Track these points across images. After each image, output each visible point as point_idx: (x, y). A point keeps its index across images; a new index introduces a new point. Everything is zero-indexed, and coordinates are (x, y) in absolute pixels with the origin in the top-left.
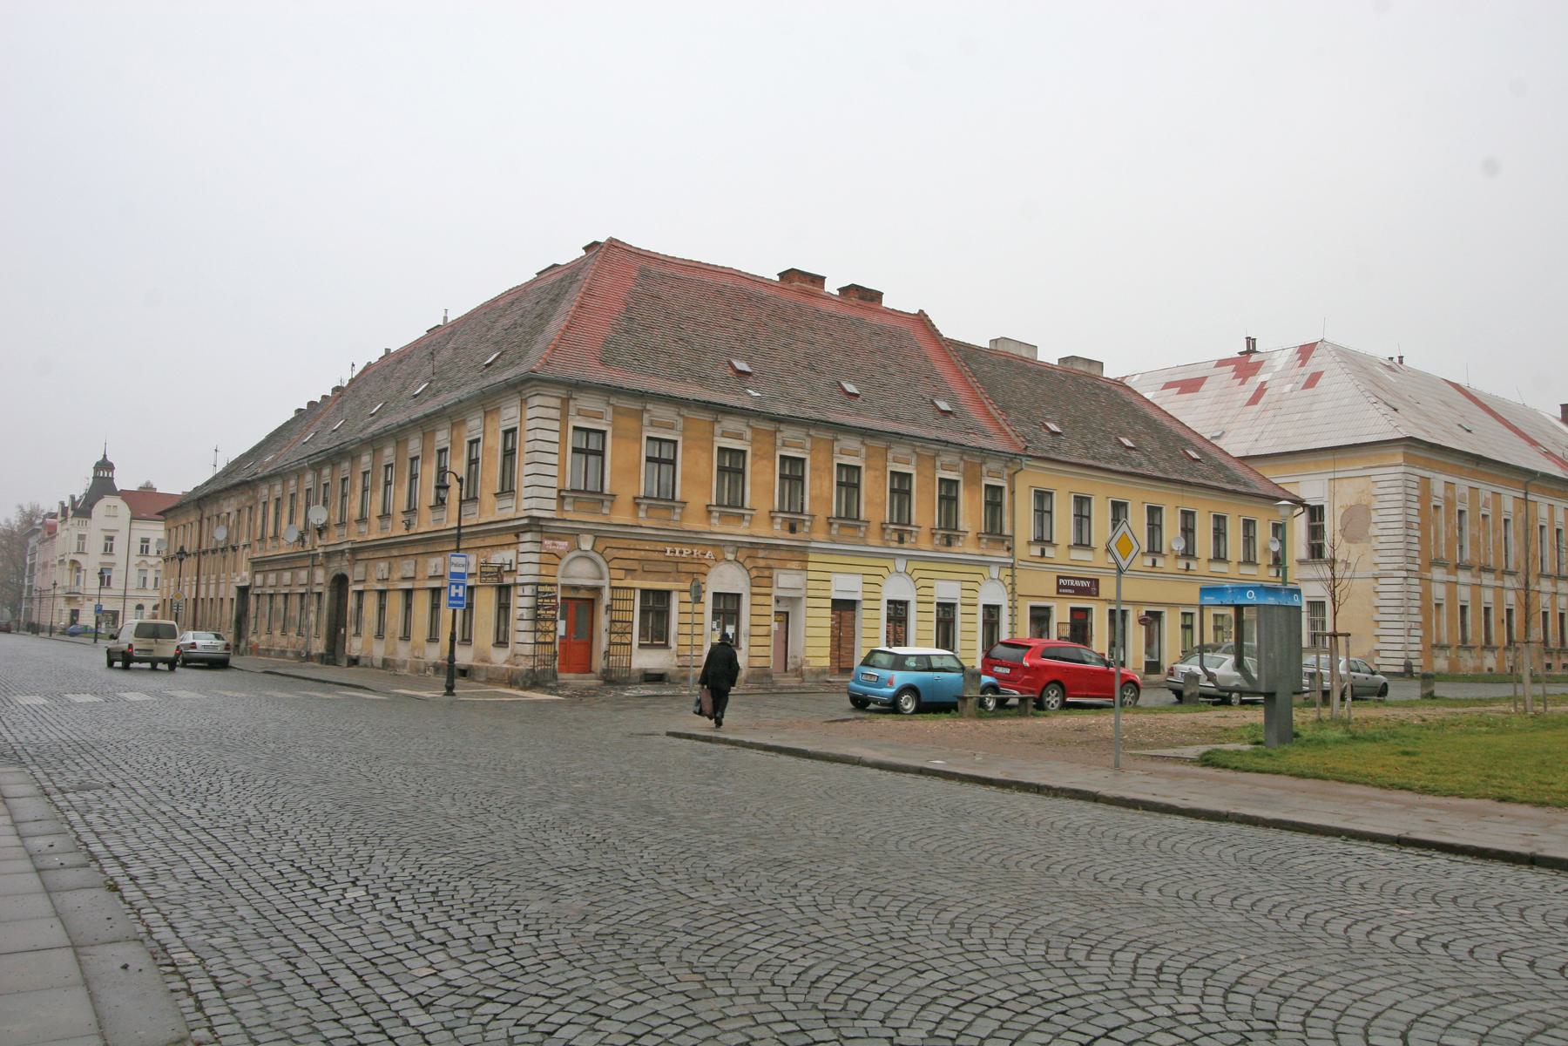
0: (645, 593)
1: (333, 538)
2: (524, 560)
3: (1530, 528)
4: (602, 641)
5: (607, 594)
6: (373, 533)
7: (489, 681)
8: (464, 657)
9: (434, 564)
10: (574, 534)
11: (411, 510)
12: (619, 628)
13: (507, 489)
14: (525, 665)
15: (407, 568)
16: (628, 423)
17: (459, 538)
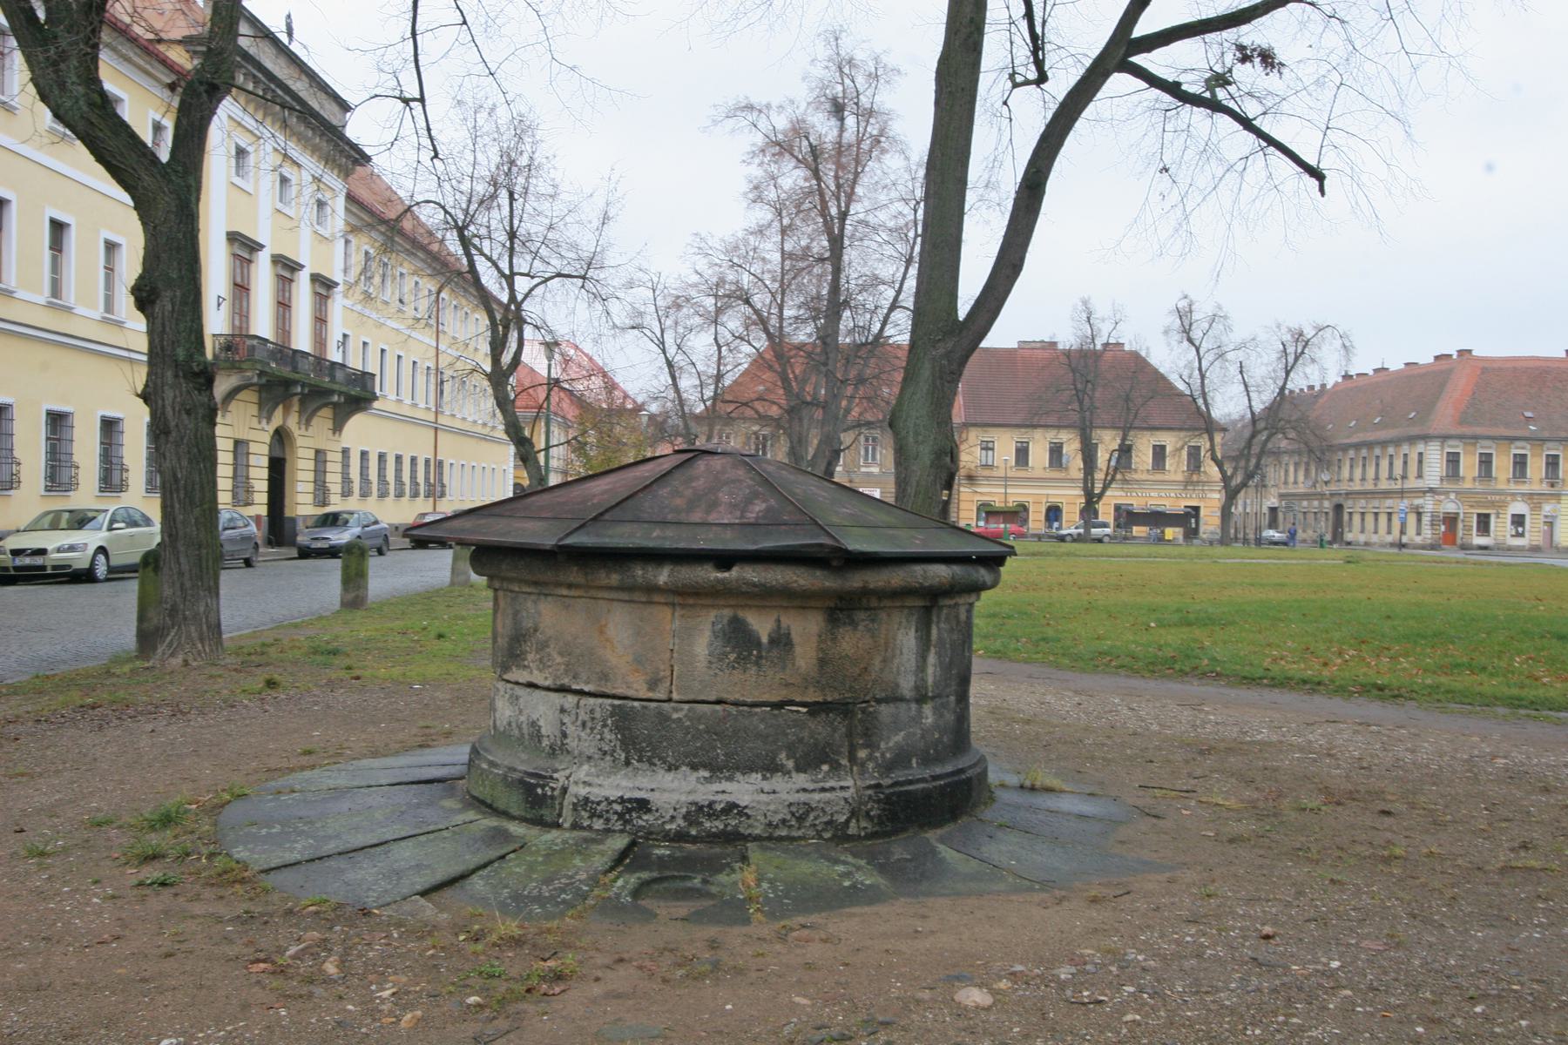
0: (1479, 515)
1: (1333, 487)
2: (1428, 504)
3: (639, 573)
4: (1460, 533)
5: (1461, 516)
6: (1357, 486)
7: (1415, 548)
8: (1405, 540)
9: (1389, 502)
10: (1447, 493)
11: (1377, 478)
12: (1468, 528)
13: (1420, 476)
14: (1429, 541)
15: (1376, 503)
16: (1470, 448)
17: (1402, 493)
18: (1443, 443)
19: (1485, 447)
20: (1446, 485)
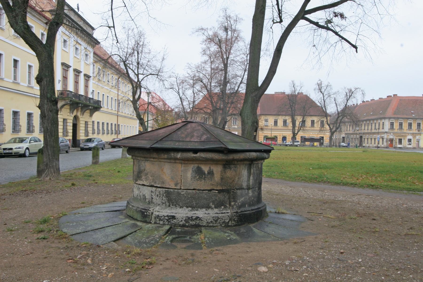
0: (399, 139)
1: (360, 132)
2: (385, 136)
3: (172, 155)
4: (394, 144)
5: (394, 139)
6: (366, 131)
7: (382, 148)
8: (379, 146)
9: (375, 136)
10: (390, 133)
11: (371, 129)
12: (396, 143)
13: (383, 128)
14: (385, 146)
15: (371, 136)
16: (397, 121)
17: (378, 133)
18: (389, 120)
19: (401, 121)
20: (390, 131)
